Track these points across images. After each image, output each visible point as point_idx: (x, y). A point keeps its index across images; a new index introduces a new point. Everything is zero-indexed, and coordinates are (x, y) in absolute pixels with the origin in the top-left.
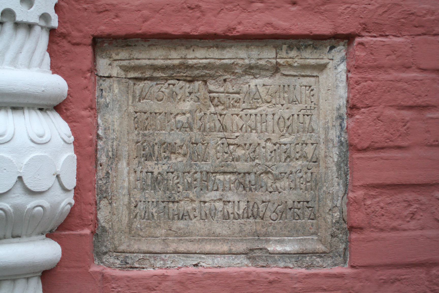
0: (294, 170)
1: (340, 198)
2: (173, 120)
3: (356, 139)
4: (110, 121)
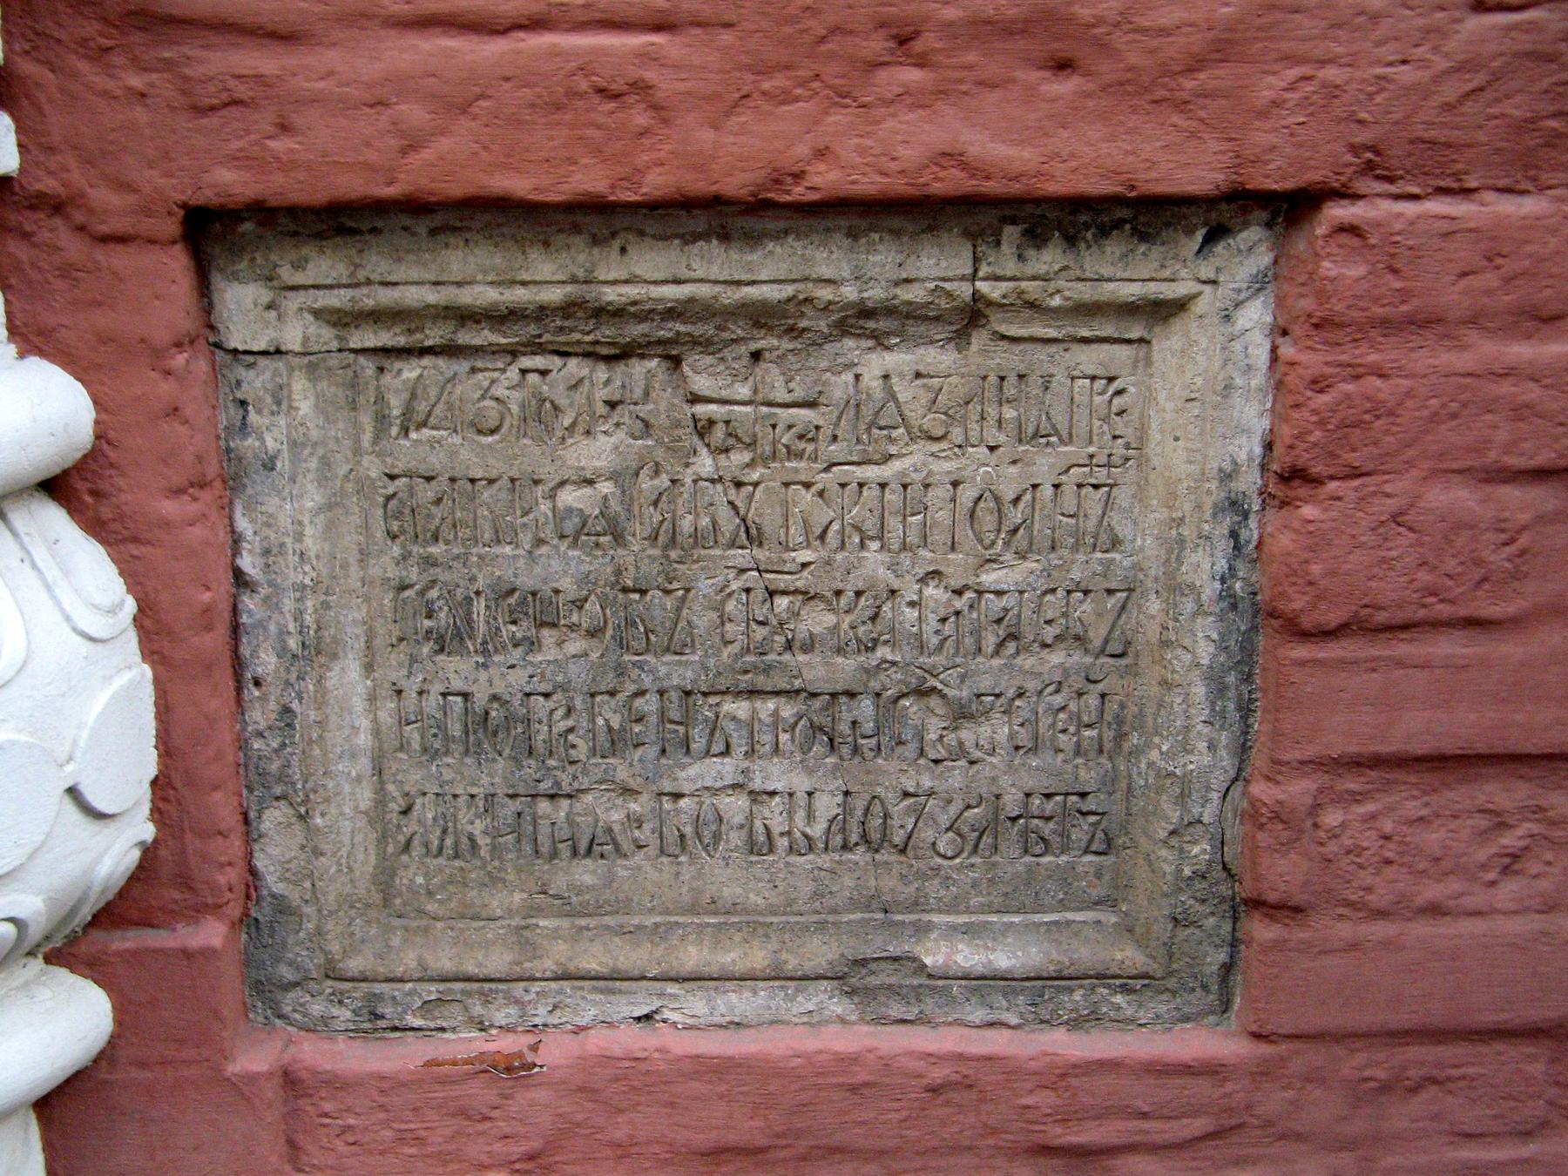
0: (1032, 685)
1: (1215, 796)
2: (545, 507)
3: (1296, 596)
4: (284, 521)
